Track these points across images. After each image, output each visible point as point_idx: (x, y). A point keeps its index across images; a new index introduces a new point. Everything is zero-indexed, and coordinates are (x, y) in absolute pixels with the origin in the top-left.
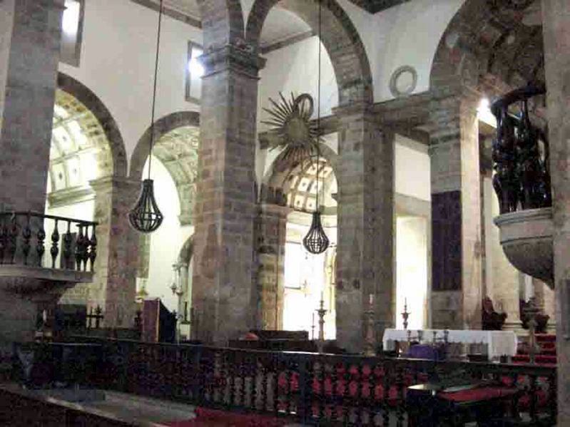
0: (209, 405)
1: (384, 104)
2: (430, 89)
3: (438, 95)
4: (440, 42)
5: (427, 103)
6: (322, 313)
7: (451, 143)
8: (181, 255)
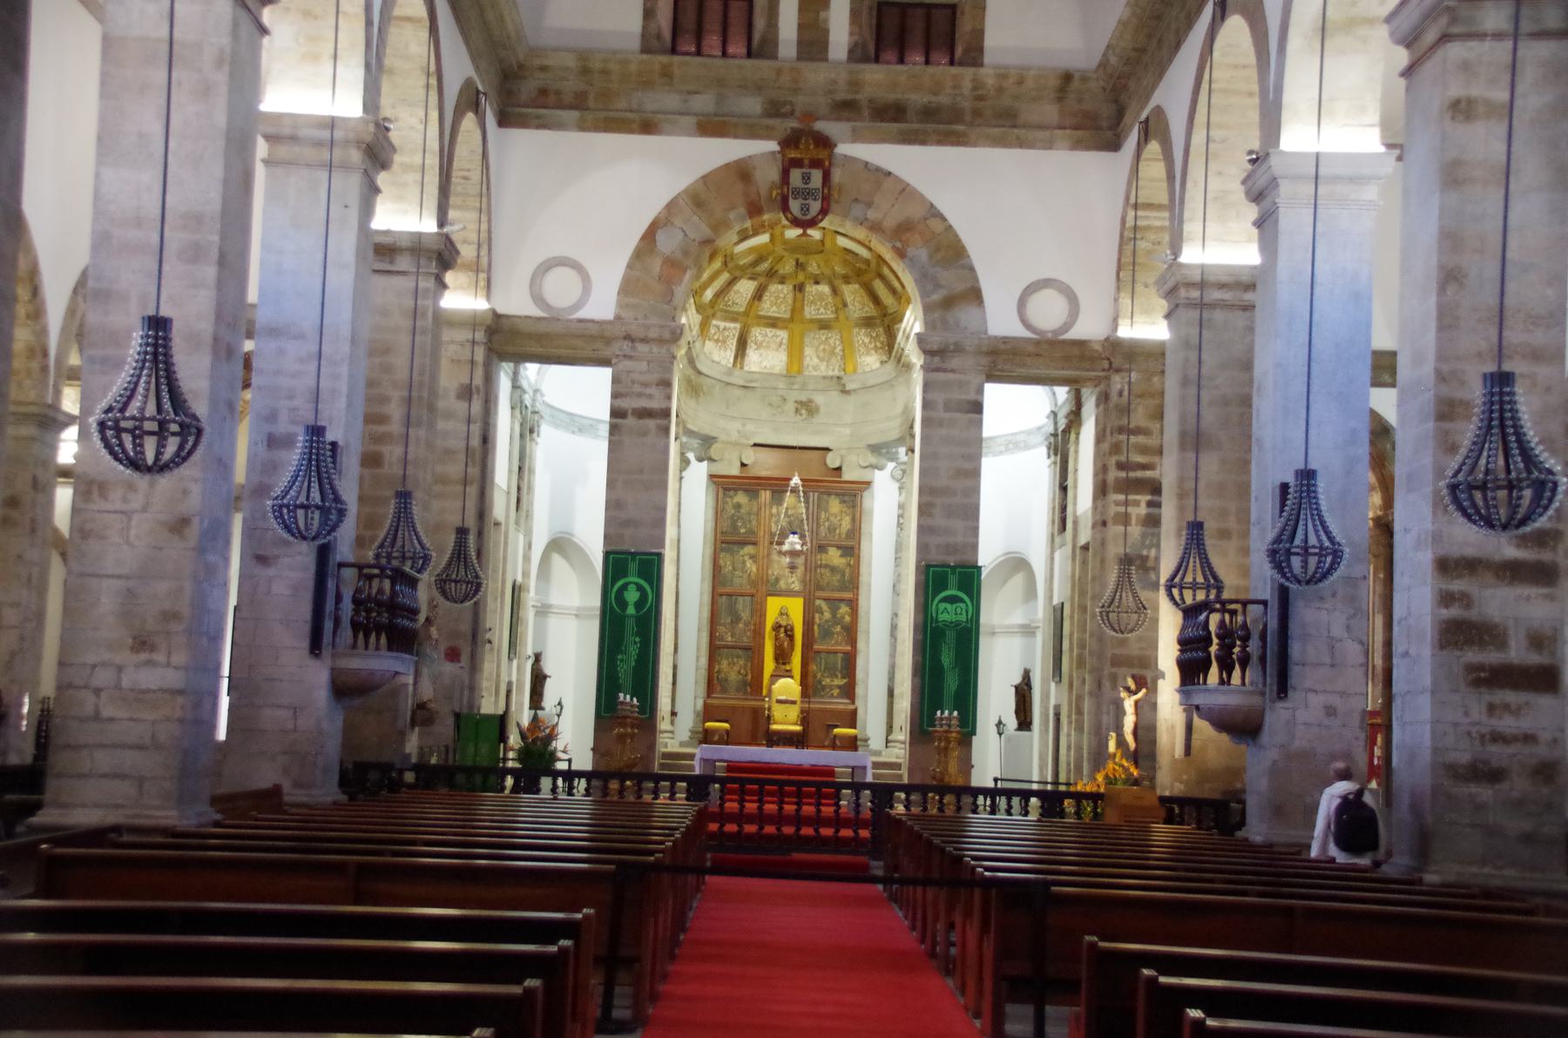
0: (1011, 446)
1: (519, 320)
2: (618, 318)
3: (636, 331)
4: (644, 238)
5: (608, 341)
6: (674, 714)
7: (651, 424)
8: (1502, 40)
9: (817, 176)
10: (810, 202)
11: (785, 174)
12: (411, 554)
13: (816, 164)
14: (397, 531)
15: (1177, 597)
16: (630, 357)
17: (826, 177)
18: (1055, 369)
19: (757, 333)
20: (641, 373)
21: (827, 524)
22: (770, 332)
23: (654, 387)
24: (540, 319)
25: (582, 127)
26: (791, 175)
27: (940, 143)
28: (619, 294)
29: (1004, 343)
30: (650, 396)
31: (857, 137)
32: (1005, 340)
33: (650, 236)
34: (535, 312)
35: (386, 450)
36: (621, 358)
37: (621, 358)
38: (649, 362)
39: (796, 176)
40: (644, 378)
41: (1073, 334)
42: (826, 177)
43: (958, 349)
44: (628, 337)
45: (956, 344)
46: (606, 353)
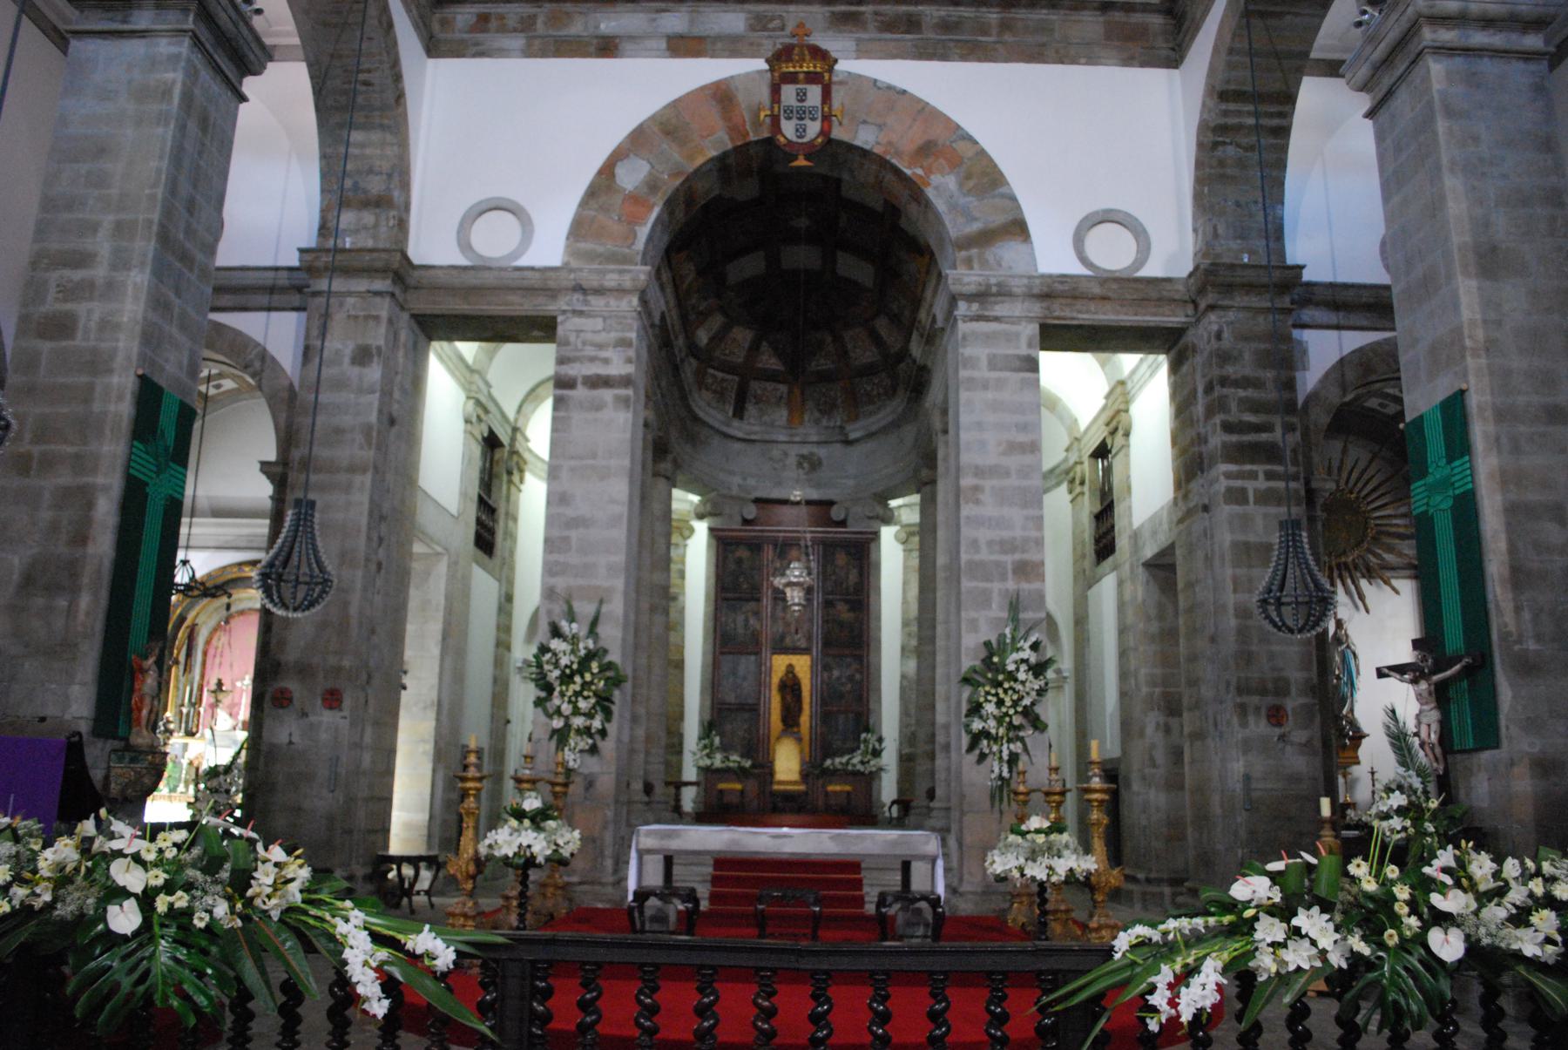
4: (600, 172)
9: (814, 93)
10: (807, 122)
11: (775, 91)
12: (307, 579)
13: (813, 78)
14: (292, 548)
15: (1274, 615)
16: (580, 313)
17: (826, 96)
18: (1126, 314)
19: (755, 386)
20: (594, 332)
21: (833, 578)
22: (770, 386)
23: (611, 349)
24: (465, 268)
25: (528, 53)
26: (783, 92)
27: (964, 58)
28: (568, 238)
29: (1062, 283)
30: (606, 361)
31: (862, 53)
32: (1063, 278)
33: (607, 171)
34: (461, 261)
35: (81, 308)
36: (569, 315)
37: (569, 315)
38: (605, 319)
39: (789, 93)
40: (602, 338)
41: (1146, 272)
42: (826, 96)
43: (1004, 293)
44: (579, 288)
45: (999, 285)
46: (551, 308)
